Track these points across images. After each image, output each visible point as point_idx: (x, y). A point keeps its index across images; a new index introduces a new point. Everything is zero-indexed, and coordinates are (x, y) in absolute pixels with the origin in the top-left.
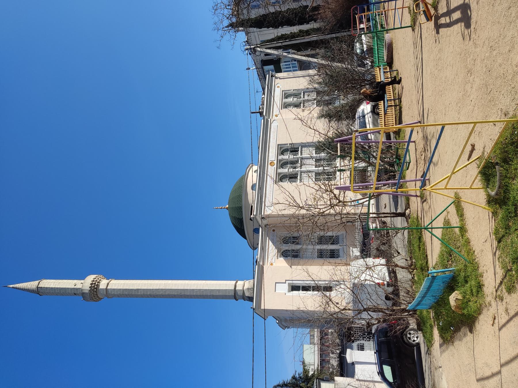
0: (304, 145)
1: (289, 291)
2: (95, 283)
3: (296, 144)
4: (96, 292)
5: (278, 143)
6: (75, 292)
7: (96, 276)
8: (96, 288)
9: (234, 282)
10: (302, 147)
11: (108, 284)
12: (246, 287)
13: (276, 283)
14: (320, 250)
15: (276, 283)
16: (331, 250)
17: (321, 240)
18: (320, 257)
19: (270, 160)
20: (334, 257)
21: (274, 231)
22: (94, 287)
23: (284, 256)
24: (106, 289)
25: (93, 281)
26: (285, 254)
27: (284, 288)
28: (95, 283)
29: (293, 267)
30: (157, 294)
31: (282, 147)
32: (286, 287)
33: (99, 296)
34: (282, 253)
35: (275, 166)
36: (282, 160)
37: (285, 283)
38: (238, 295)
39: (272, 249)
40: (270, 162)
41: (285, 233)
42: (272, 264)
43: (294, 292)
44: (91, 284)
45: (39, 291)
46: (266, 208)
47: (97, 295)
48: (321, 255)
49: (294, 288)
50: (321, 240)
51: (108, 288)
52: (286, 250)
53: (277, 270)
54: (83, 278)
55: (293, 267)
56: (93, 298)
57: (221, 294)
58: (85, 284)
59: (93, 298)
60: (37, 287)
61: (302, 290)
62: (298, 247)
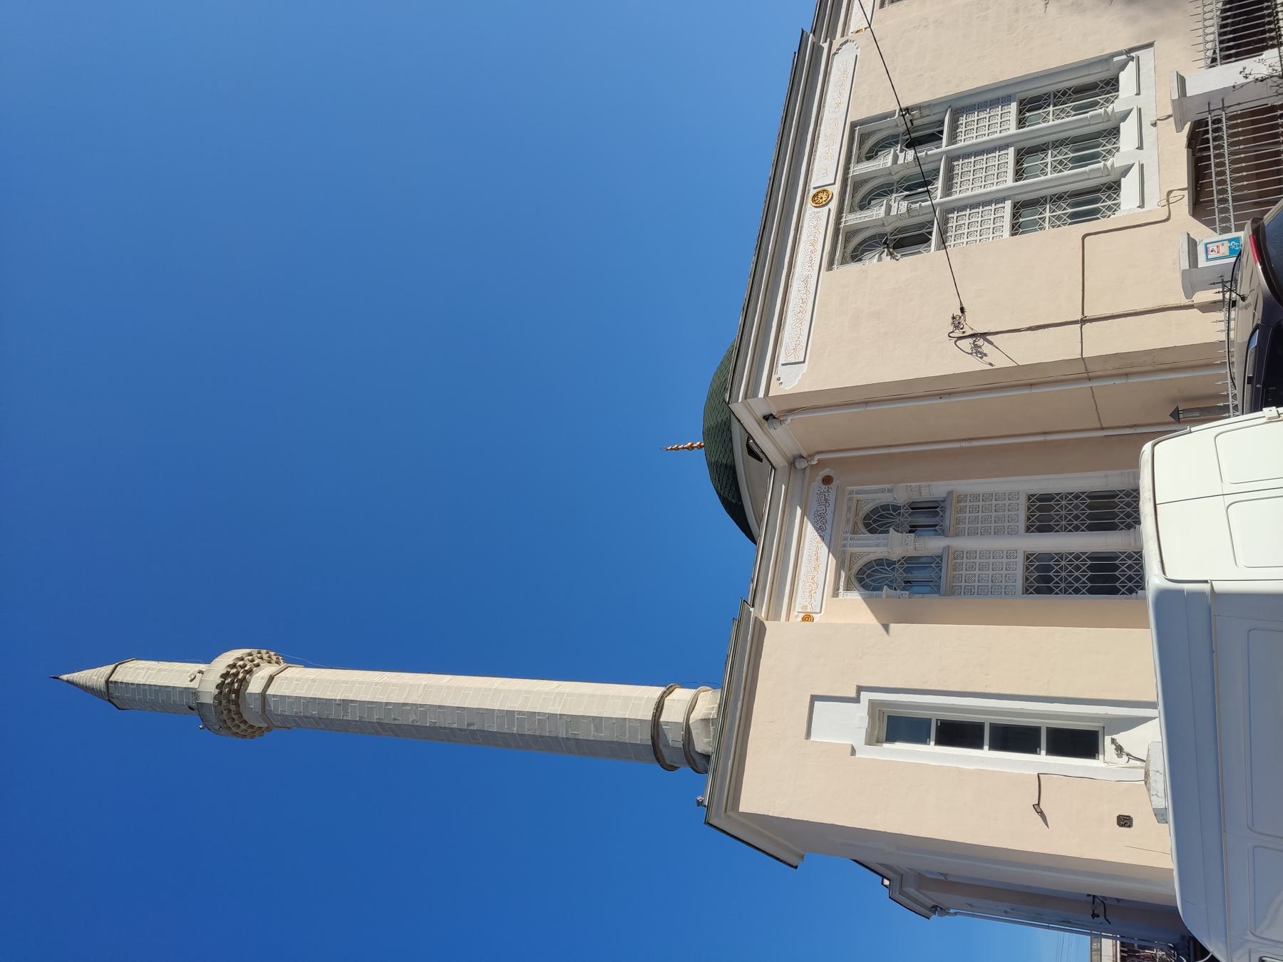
0: (963, 106)
1: (873, 740)
2: (237, 674)
3: (919, 107)
4: (236, 703)
5: (853, 117)
6: (188, 702)
7: (248, 651)
8: (237, 692)
9: (657, 691)
10: (957, 113)
11: (271, 678)
12: (695, 716)
13: (814, 698)
14: (1040, 557)
15: (814, 698)
16: (1094, 557)
17: (1044, 513)
18: (1038, 591)
19: (812, 185)
20: (1114, 591)
21: (827, 480)
22: (233, 686)
23: (865, 587)
24: (263, 695)
25: (234, 666)
26: (869, 578)
27: (847, 725)
28: (237, 674)
29: (893, 626)
30: (401, 721)
31: (869, 134)
32: (858, 716)
33: (245, 717)
34: (861, 571)
35: (833, 205)
36: (866, 181)
37: (857, 700)
38: (667, 745)
39: (812, 558)
40: (812, 192)
41: (876, 493)
42: (807, 618)
43: (899, 746)
44: (225, 676)
45: (110, 693)
46: (781, 371)
47: (239, 713)
48: (1045, 579)
49: (899, 726)
50: (1044, 513)
51: (270, 691)
52: (880, 562)
53: (822, 634)
54: (208, 660)
55: (893, 626)
56: (229, 722)
57: (605, 735)
58: (198, 677)
59: (229, 722)
60: (107, 682)
61: (993, 747)
62: (931, 545)
